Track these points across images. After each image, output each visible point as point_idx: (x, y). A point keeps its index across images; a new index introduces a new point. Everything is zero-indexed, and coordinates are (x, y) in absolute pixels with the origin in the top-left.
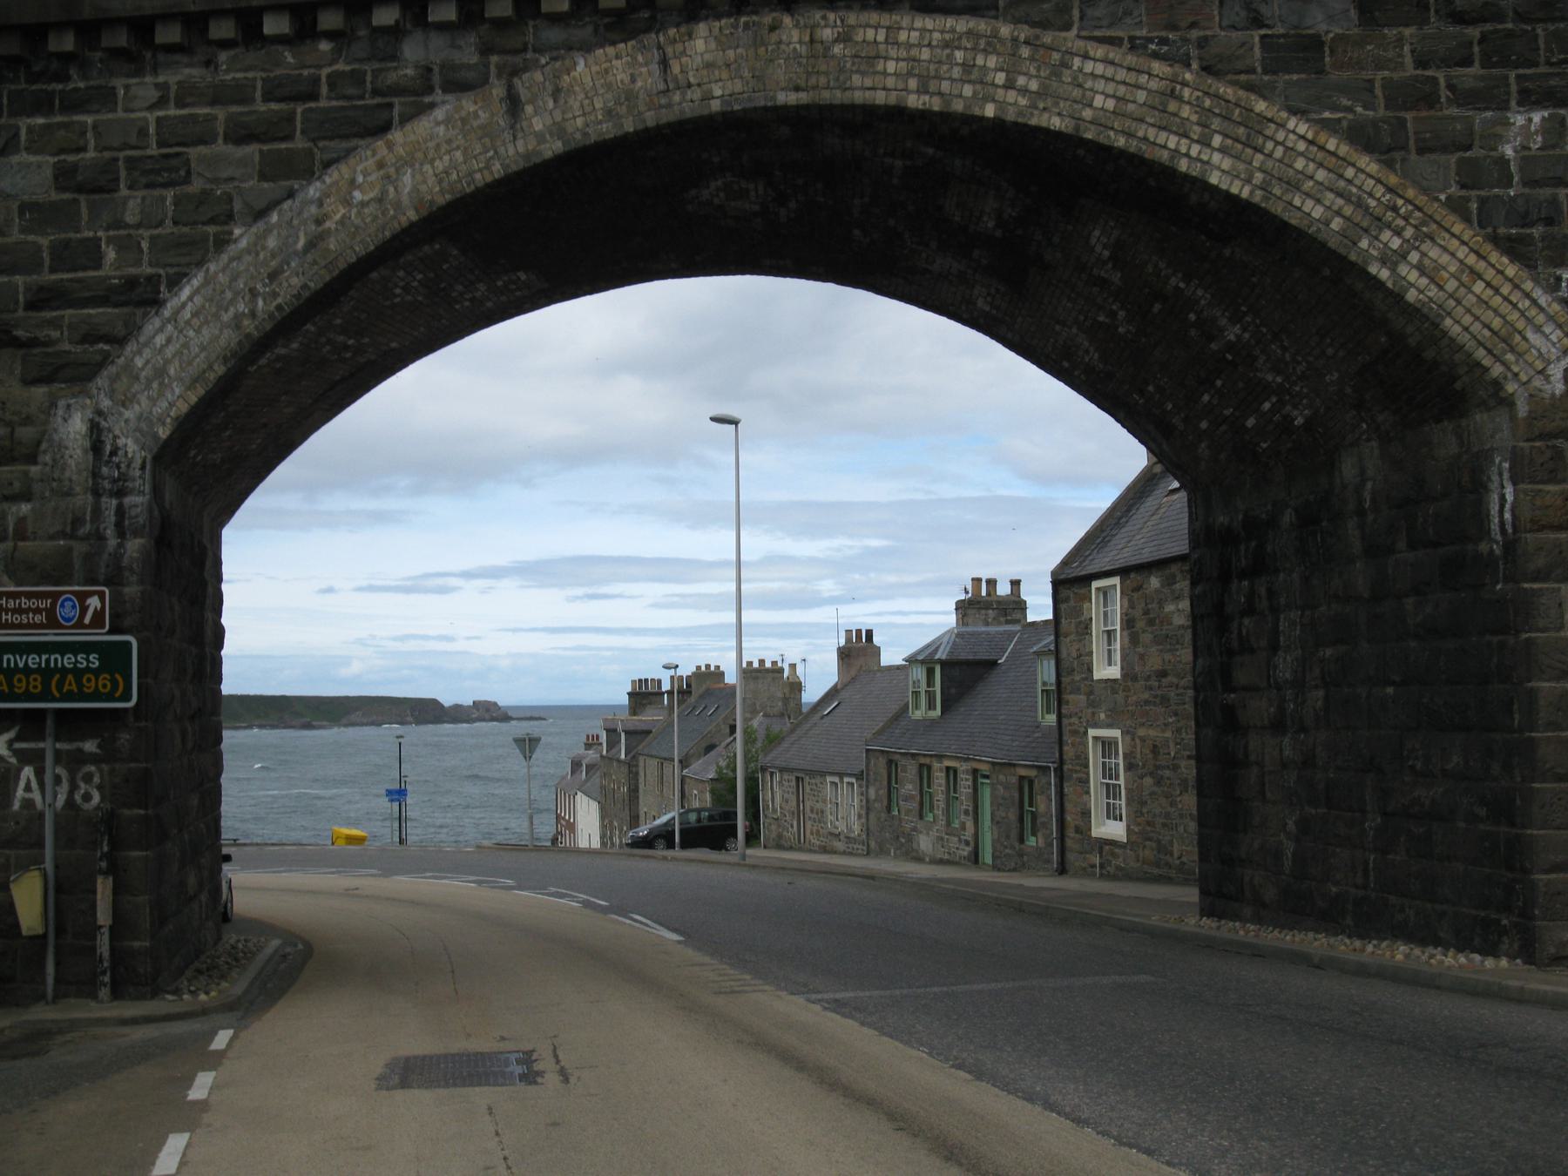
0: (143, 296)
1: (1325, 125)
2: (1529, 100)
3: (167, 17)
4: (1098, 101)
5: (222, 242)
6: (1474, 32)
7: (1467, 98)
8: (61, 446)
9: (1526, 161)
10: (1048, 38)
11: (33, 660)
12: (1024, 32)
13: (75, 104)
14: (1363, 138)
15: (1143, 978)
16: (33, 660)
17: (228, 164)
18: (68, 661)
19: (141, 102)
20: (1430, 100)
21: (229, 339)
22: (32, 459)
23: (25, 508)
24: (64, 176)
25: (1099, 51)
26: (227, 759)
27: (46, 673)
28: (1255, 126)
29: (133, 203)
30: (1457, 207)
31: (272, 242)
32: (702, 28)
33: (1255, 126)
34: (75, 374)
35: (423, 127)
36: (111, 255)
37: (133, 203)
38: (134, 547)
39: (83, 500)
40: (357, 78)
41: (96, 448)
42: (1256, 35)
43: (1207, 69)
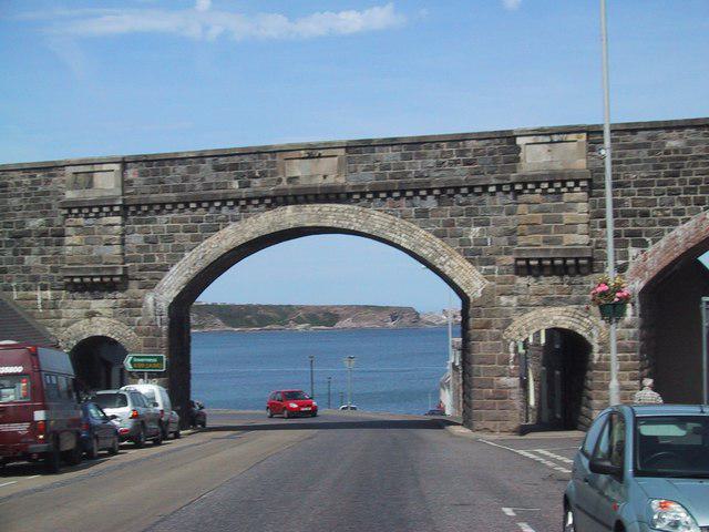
0: (165, 269)
1: (430, 231)
2: (477, 225)
3: (450, 188)
4: (377, 226)
5: (183, 256)
6: (464, 208)
7: (462, 224)
8: (147, 304)
9: (475, 240)
10: (366, 210)
11: (142, 360)
12: (360, 209)
13: (148, 222)
14: (437, 234)
15: (322, 327)
16: (142, 360)
17: (183, 237)
18: (150, 360)
19: (163, 221)
20: (453, 225)
21: (185, 279)
22: (140, 307)
23: (138, 318)
24: (146, 239)
25: (377, 213)
26: (192, 367)
27: (145, 363)
28: (413, 231)
29: (162, 246)
30: (458, 251)
31: (194, 257)
32: (289, 207)
33: (413, 231)
34: (149, 287)
35: (227, 230)
36: (157, 258)
37: (162, 246)
38: (165, 328)
39: (152, 316)
40: (211, 217)
41: (155, 305)
42: (413, 209)
43: (403, 218)
